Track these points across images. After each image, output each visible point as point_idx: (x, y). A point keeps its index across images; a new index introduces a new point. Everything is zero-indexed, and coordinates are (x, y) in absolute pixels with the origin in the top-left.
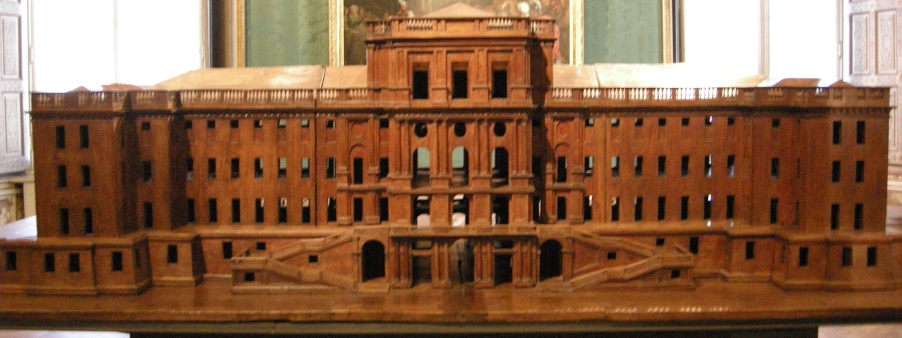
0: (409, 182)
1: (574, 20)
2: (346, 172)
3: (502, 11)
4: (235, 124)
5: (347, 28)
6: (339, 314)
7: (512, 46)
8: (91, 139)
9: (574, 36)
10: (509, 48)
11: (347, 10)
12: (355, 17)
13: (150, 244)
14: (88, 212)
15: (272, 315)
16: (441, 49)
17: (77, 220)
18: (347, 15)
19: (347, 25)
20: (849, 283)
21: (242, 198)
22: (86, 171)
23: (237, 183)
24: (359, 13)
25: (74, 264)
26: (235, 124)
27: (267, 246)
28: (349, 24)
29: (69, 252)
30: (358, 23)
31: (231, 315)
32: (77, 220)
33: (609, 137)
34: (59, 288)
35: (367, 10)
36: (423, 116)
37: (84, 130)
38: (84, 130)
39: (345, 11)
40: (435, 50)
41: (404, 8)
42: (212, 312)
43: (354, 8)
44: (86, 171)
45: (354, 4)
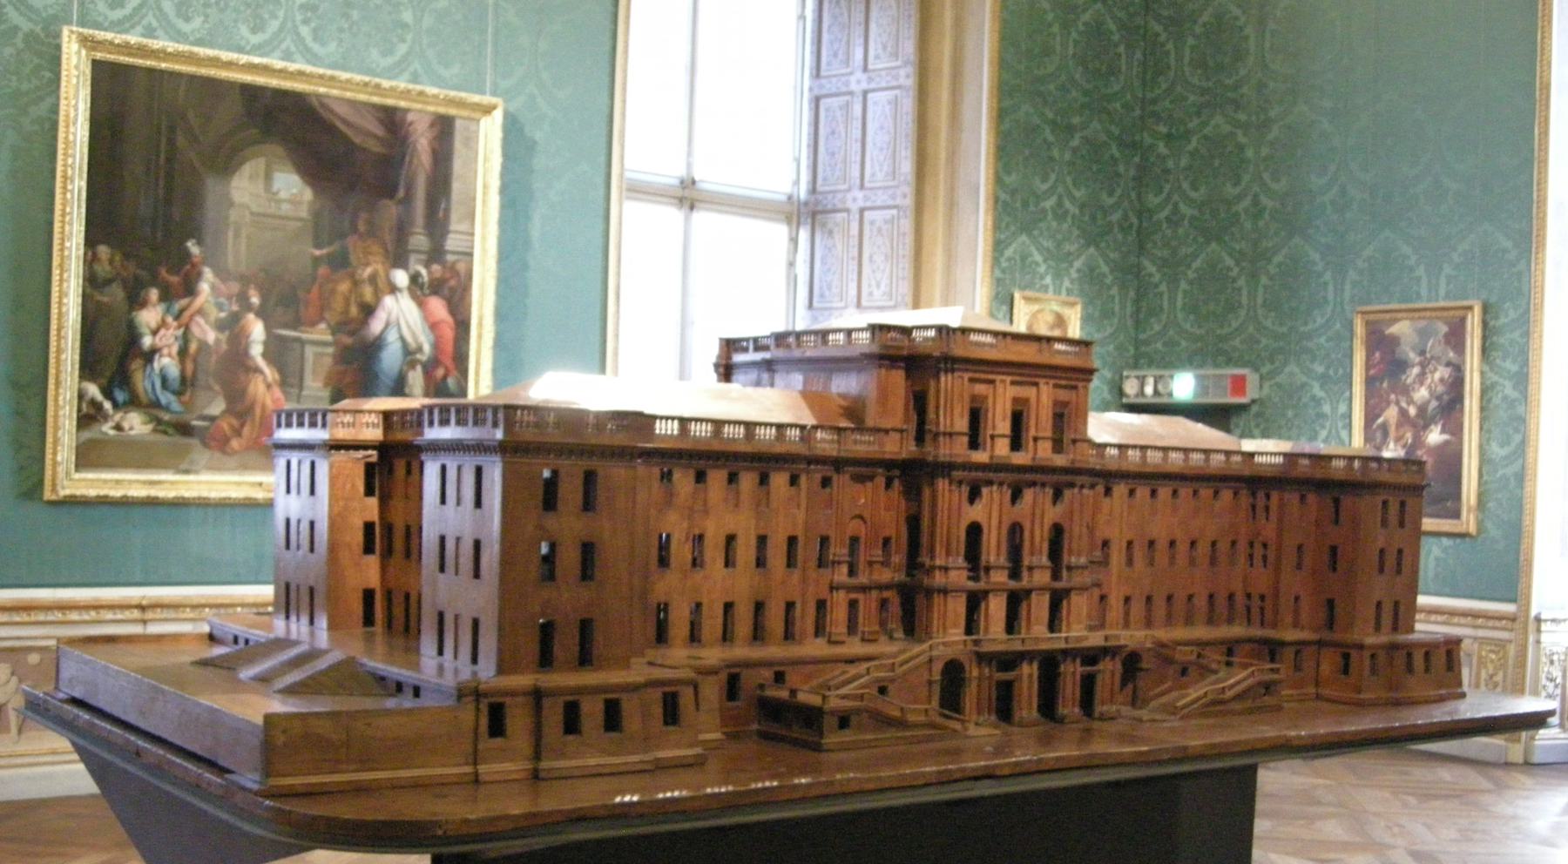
0: (1006, 572)
1: (481, 307)
2: (847, 559)
3: (363, 282)
4: (700, 477)
5: (88, 290)
6: (1194, 747)
7: (1077, 379)
8: (601, 495)
9: (480, 336)
10: (1073, 383)
11: (90, 254)
12: (103, 269)
13: (1544, 627)
14: (585, 627)
15: (1322, 735)
16: (1004, 377)
17: (567, 643)
18: (90, 261)
19: (87, 284)
20: (1410, 694)
21: (705, 601)
22: (588, 550)
23: (698, 575)
24: (111, 262)
25: (612, 718)
26: (700, 477)
27: (787, 677)
28: (92, 281)
29: (603, 696)
30: (108, 282)
31: (930, 773)
32: (567, 643)
33: (1125, 514)
34: (592, 762)
35: (126, 256)
36: (980, 474)
37: (590, 478)
38: (590, 478)
39: (85, 254)
40: (999, 378)
41: (195, 260)
42: (908, 771)
43: (103, 251)
44: (588, 550)
45: (103, 243)
